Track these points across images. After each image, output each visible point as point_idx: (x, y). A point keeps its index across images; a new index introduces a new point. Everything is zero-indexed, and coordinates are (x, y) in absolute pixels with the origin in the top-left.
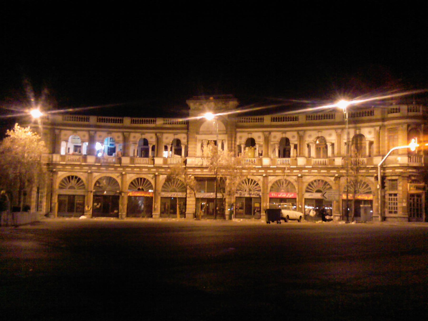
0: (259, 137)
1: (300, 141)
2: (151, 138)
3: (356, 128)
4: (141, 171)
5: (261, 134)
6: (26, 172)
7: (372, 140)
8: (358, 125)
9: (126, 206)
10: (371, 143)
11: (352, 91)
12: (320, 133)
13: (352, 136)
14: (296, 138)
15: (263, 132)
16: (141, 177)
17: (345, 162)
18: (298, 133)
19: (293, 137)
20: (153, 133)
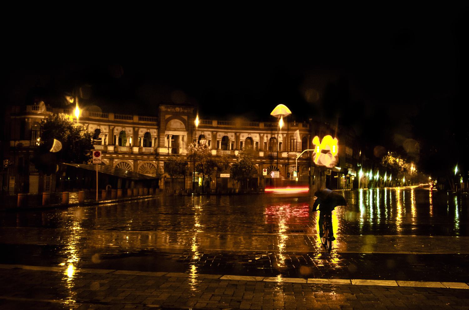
0: (209, 135)
1: (237, 139)
2: (231, 137)
3: (272, 134)
4: (148, 158)
5: (210, 133)
6: (244, 159)
7: (282, 142)
8: (273, 132)
9: (203, 275)
10: (257, 143)
11: (85, 108)
12: (226, 134)
13: (269, 138)
14: (234, 138)
15: (212, 132)
16: (118, 163)
17: (186, 164)
18: (260, 135)
19: (232, 136)
20: (131, 127)
